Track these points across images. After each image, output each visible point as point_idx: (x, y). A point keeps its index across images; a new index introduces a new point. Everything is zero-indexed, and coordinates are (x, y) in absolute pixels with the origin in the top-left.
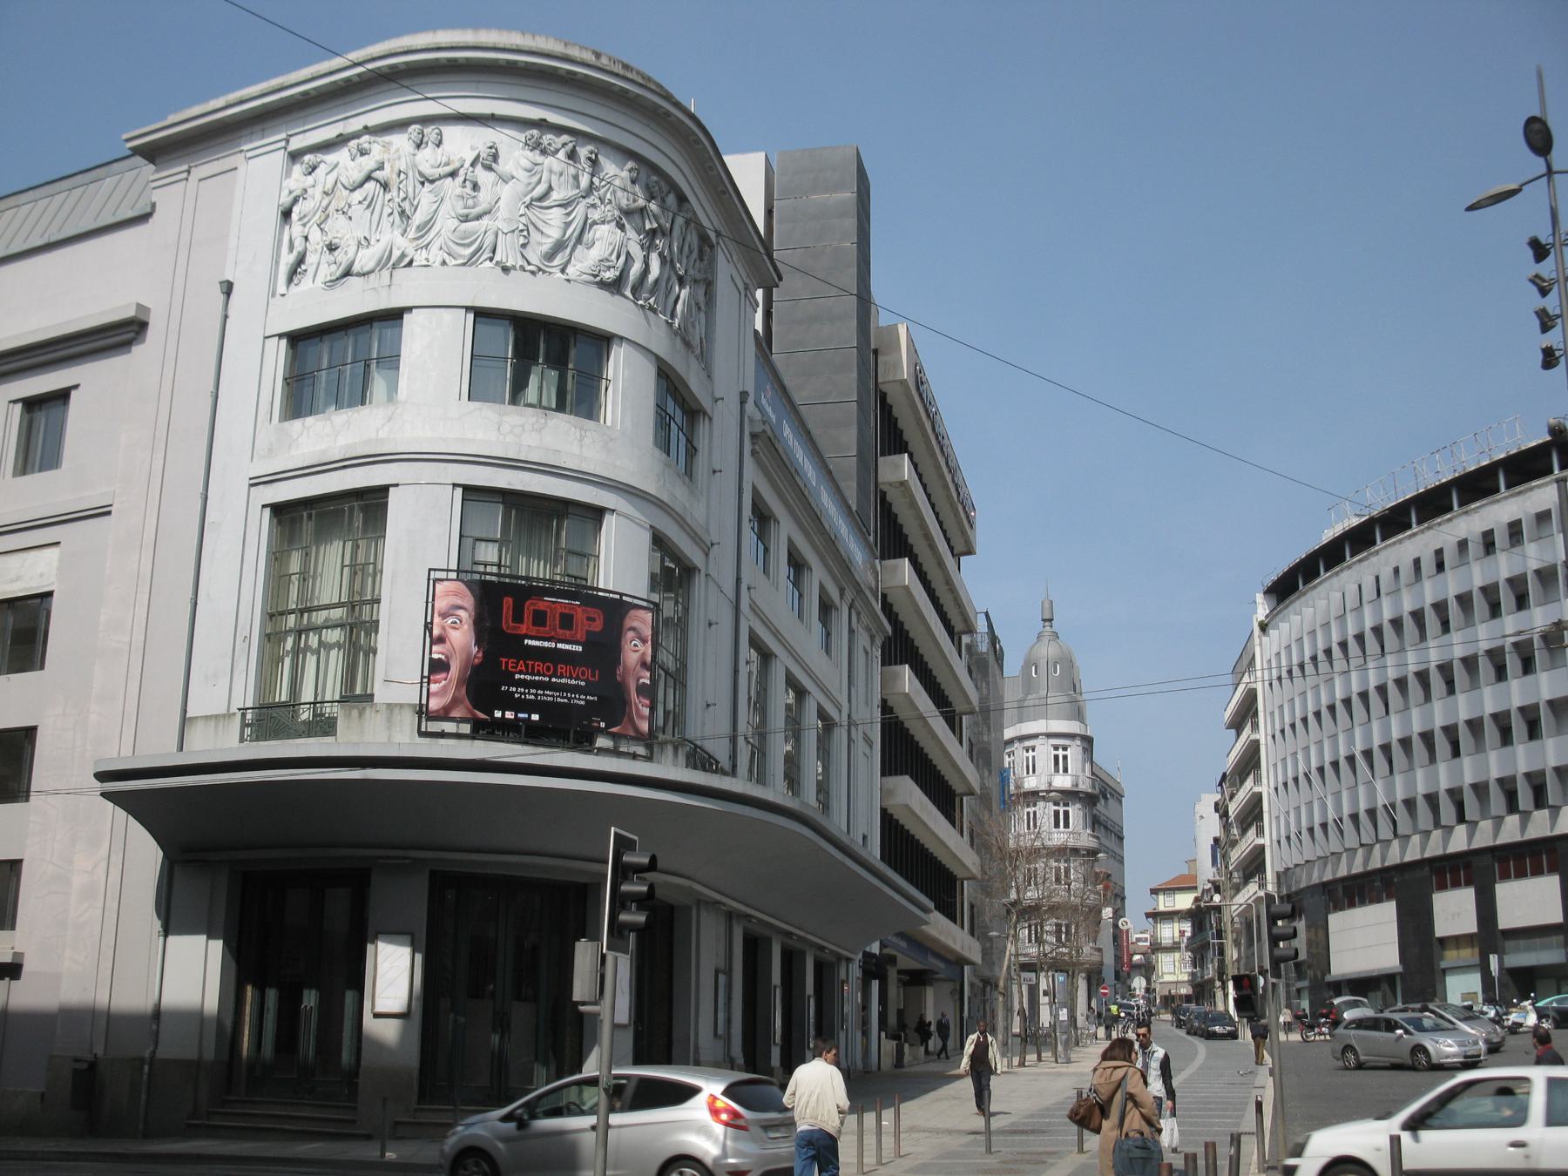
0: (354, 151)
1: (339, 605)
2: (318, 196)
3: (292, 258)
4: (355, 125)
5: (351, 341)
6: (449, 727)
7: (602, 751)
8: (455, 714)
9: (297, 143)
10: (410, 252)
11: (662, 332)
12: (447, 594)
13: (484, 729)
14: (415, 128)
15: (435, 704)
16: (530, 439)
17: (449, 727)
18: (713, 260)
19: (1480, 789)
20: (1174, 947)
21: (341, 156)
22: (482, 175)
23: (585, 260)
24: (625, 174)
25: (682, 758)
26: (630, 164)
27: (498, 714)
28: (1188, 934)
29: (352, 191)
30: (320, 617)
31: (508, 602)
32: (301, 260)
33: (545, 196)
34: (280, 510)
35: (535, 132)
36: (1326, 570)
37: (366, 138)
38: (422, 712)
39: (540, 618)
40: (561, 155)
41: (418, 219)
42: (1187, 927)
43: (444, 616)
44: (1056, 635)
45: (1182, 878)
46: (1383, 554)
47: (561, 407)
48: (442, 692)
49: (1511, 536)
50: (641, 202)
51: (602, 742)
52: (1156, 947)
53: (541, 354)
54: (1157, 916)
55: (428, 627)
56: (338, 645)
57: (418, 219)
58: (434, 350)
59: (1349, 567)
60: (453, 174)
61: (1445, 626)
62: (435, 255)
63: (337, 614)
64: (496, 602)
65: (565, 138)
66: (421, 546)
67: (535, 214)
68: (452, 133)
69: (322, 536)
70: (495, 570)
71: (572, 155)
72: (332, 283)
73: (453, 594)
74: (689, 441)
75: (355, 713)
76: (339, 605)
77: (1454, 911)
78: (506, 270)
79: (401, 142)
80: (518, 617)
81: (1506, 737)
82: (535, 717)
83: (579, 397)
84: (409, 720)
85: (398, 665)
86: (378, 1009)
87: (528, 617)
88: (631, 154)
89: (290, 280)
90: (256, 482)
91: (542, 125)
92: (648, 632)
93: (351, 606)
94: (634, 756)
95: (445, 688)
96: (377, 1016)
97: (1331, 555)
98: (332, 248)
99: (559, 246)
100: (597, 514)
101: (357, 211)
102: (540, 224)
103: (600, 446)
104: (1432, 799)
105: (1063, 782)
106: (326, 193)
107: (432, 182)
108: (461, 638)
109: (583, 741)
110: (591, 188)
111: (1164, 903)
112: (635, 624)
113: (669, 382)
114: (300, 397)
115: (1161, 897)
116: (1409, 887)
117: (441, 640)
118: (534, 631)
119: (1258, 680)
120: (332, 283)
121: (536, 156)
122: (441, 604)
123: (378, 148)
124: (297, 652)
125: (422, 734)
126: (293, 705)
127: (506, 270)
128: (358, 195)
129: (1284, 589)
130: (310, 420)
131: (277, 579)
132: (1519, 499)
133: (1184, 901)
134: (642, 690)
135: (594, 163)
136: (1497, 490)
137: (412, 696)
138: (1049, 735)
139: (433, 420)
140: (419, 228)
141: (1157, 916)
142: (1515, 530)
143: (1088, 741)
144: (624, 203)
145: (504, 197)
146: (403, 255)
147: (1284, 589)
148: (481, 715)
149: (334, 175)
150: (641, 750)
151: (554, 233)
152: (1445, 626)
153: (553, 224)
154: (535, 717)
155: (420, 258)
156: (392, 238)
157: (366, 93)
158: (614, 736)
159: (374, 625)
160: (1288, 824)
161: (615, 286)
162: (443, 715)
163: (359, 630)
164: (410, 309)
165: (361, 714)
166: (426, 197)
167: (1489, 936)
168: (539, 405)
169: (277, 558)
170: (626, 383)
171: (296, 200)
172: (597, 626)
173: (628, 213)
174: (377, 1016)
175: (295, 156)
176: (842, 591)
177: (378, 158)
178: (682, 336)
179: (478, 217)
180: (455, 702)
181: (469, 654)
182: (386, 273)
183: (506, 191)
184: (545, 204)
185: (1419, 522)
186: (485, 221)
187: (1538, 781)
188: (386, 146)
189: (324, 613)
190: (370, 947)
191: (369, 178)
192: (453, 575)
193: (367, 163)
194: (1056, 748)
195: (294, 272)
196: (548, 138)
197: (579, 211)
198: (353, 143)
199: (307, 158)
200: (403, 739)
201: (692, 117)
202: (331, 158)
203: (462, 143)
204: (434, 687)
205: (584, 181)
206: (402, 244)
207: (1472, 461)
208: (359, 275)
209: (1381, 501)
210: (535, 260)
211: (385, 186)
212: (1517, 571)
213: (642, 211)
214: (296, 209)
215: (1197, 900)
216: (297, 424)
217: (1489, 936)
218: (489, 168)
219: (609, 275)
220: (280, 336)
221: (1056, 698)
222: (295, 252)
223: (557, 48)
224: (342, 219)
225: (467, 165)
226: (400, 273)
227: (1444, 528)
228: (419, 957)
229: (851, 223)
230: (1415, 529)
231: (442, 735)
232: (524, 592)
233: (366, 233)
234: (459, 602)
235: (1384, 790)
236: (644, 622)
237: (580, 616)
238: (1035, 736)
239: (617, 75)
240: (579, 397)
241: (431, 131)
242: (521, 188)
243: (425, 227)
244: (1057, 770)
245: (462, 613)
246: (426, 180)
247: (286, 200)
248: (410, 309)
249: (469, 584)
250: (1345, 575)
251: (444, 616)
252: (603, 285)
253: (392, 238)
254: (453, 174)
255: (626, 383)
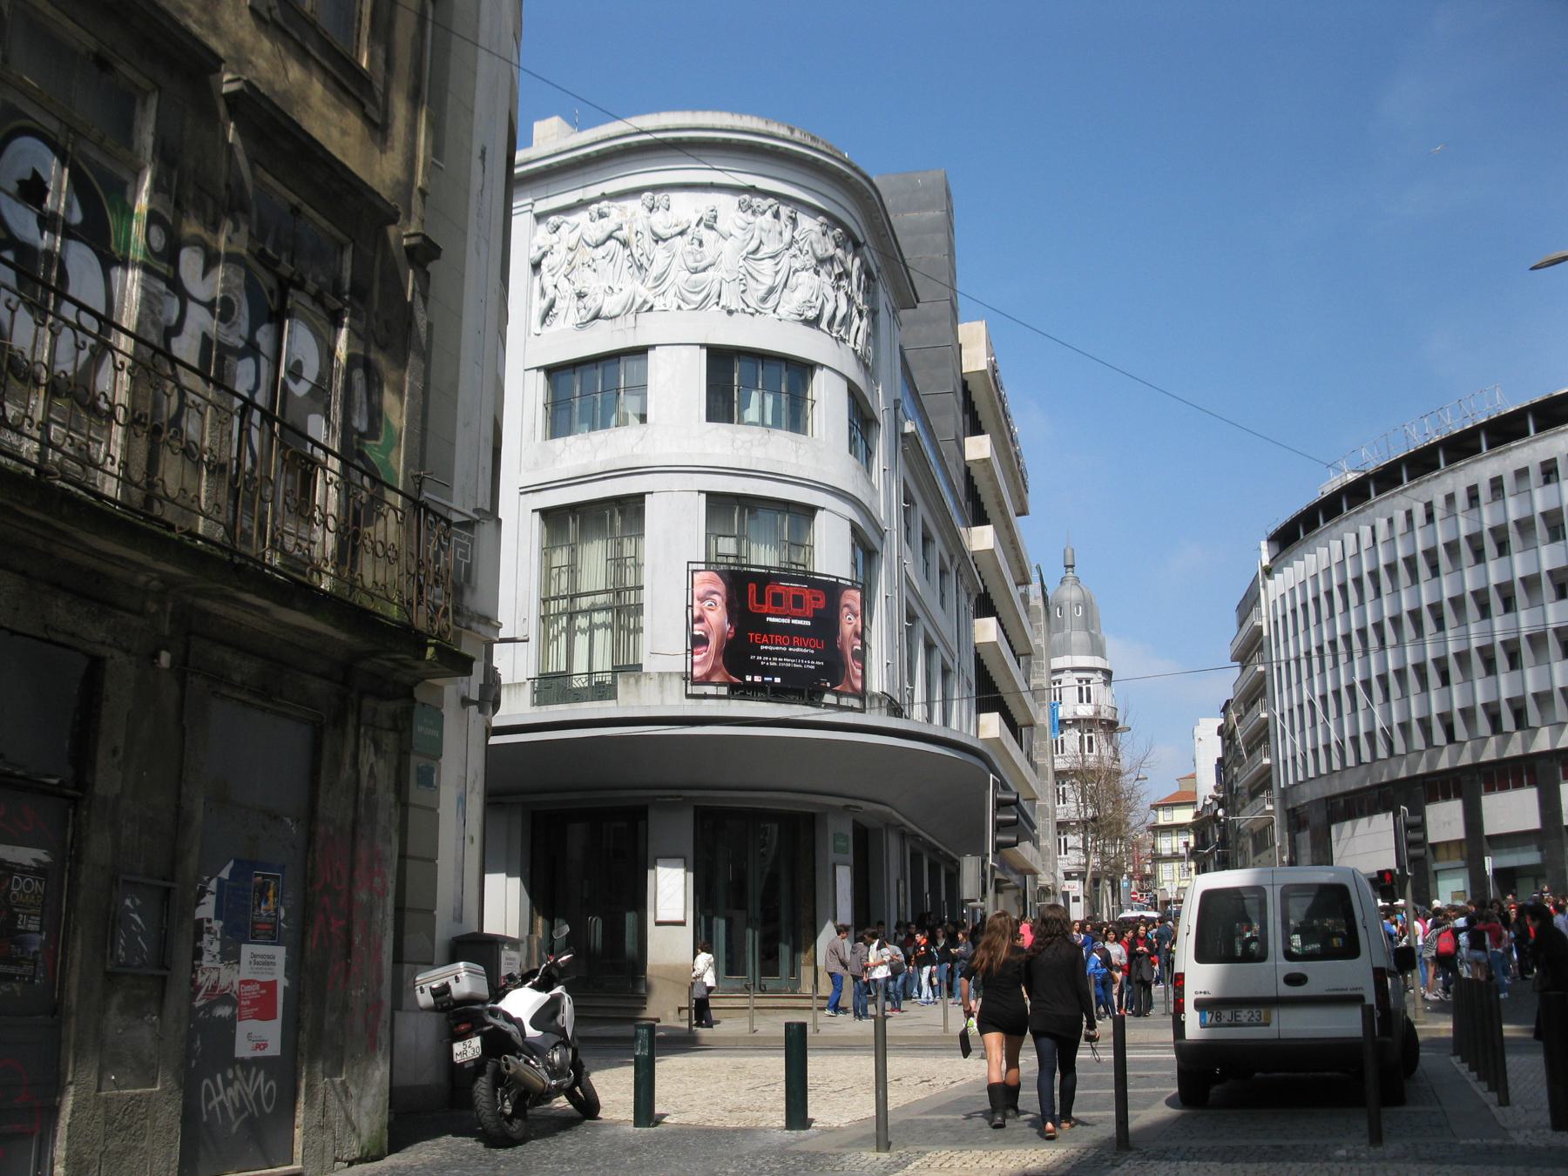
0: (595, 215)
1: (607, 591)
2: (564, 251)
3: (545, 303)
4: (593, 192)
5: (600, 371)
6: (711, 690)
7: (828, 706)
8: (715, 679)
9: (541, 206)
10: (651, 300)
11: (851, 358)
12: (703, 582)
13: (740, 691)
14: (647, 195)
15: (698, 672)
16: (758, 452)
17: (711, 690)
18: (875, 292)
19: (1468, 714)
20: (1175, 857)
21: (582, 217)
22: (703, 231)
23: (791, 302)
24: (818, 229)
25: (885, 711)
26: (821, 219)
27: (748, 678)
28: (1192, 845)
29: (597, 246)
30: (584, 603)
31: (752, 587)
32: (552, 306)
33: (755, 251)
34: (547, 514)
35: (747, 197)
36: (1326, 521)
37: (604, 203)
38: (688, 678)
39: (777, 599)
40: (769, 213)
41: (655, 270)
42: (1191, 839)
43: (702, 600)
44: (1077, 579)
45: (1179, 794)
46: (1377, 507)
47: (776, 424)
48: (704, 661)
49: (1493, 490)
50: (831, 251)
51: (829, 698)
52: (1157, 858)
53: (732, 375)
54: (1159, 830)
55: (690, 607)
56: (605, 625)
57: (655, 270)
58: (677, 381)
59: (1347, 518)
60: (682, 233)
61: (1435, 570)
62: (671, 301)
63: (600, 599)
64: (742, 587)
65: (771, 201)
66: (674, 544)
67: (752, 265)
68: (677, 198)
69: (585, 535)
70: (731, 560)
71: (776, 215)
72: (582, 325)
73: (707, 582)
74: (867, 448)
75: (632, 680)
76: (607, 591)
77: (1445, 820)
78: (730, 312)
79: (634, 206)
80: (761, 599)
81: (1490, 666)
82: (778, 680)
83: (795, 417)
84: (677, 686)
85: (664, 640)
86: (659, 919)
87: (769, 599)
88: (821, 212)
89: (543, 322)
90: (526, 491)
91: (752, 190)
92: (858, 608)
93: (618, 593)
94: (852, 709)
95: (705, 660)
96: (658, 924)
97: (1330, 508)
98: (581, 296)
99: (771, 291)
100: (810, 511)
101: (601, 264)
102: (755, 274)
103: (809, 455)
104: (1425, 724)
105: (1085, 711)
106: (571, 249)
107: (665, 240)
108: (717, 617)
109: (812, 696)
110: (793, 241)
111: (1163, 818)
112: (848, 602)
113: (854, 394)
114: (559, 420)
115: (1161, 813)
116: (1404, 797)
117: (700, 619)
118: (773, 610)
119: (1263, 618)
120: (582, 325)
121: (749, 217)
122: (699, 590)
123: (615, 210)
124: (571, 632)
125: (688, 696)
126: (567, 675)
127: (730, 312)
128: (601, 251)
129: (1287, 538)
130: (570, 439)
131: (547, 570)
132: (1500, 458)
133: (1185, 816)
134: (855, 655)
135: (794, 221)
136: (1479, 450)
137: (679, 665)
138: (1074, 670)
139: (673, 440)
140: (656, 279)
141: (1159, 830)
142: (1497, 484)
143: (1108, 673)
144: (819, 253)
145: (726, 252)
146: (645, 302)
147: (1287, 538)
148: (736, 680)
149: (577, 233)
150: (856, 703)
151: (768, 282)
152: (1435, 570)
153: (766, 273)
154: (778, 680)
155: (659, 304)
156: (633, 287)
157: (602, 165)
158: (838, 694)
159: (638, 609)
160: (1293, 746)
161: (814, 323)
162: (705, 680)
163: (625, 610)
164: (653, 347)
165: (637, 681)
166: (660, 253)
167: (1476, 841)
168: (763, 423)
169: (547, 551)
170: (827, 400)
171: (544, 255)
172: (821, 604)
173: (821, 261)
174: (658, 924)
175: (540, 218)
176: (952, 557)
177: (619, 221)
178: (861, 360)
179: (704, 270)
180: (714, 669)
181: (723, 629)
182: (631, 317)
183: (728, 247)
184: (759, 256)
185: (1410, 479)
186: (711, 271)
187: (1518, 706)
188: (622, 210)
189: (590, 599)
190: (650, 873)
191: (610, 237)
192: (702, 567)
193: (608, 225)
194: (1080, 681)
195: (546, 315)
196: (757, 201)
197: (785, 261)
198: (594, 207)
199: (552, 219)
200: (674, 702)
201: (848, 164)
202: (573, 219)
203: (686, 207)
204: (697, 658)
205: (787, 237)
206: (644, 292)
207: (1455, 425)
208: (606, 318)
209: (1374, 460)
210: (753, 303)
211: (625, 244)
212: (1499, 521)
213: (831, 259)
214: (544, 262)
215: (1197, 814)
216: (559, 442)
217: (1476, 841)
218: (711, 228)
219: (811, 314)
220: (538, 369)
221: (1078, 637)
222: (547, 299)
223: (783, 131)
224: (588, 272)
225: (693, 225)
226: (643, 317)
227: (1433, 483)
228: (691, 875)
229: (941, 238)
230: (1406, 484)
231: (705, 696)
232: (764, 579)
233: (611, 284)
234: (713, 588)
235: (1378, 715)
236: (854, 599)
237: (808, 596)
238: (1062, 671)
239: (810, 148)
240: (795, 417)
241: (660, 197)
242: (737, 244)
243: (660, 279)
244: (1081, 701)
245: (715, 597)
246: (658, 239)
247: (536, 255)
248: (653, 347)
249: (719, 573)
250: (1343, 525)
251: (702, 600)
252: (807, 322)
253: (633, 287)
254: (682, 233)
255: (827, 400)
